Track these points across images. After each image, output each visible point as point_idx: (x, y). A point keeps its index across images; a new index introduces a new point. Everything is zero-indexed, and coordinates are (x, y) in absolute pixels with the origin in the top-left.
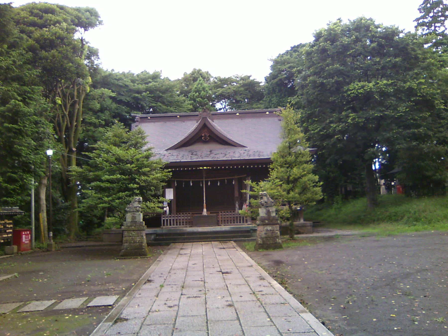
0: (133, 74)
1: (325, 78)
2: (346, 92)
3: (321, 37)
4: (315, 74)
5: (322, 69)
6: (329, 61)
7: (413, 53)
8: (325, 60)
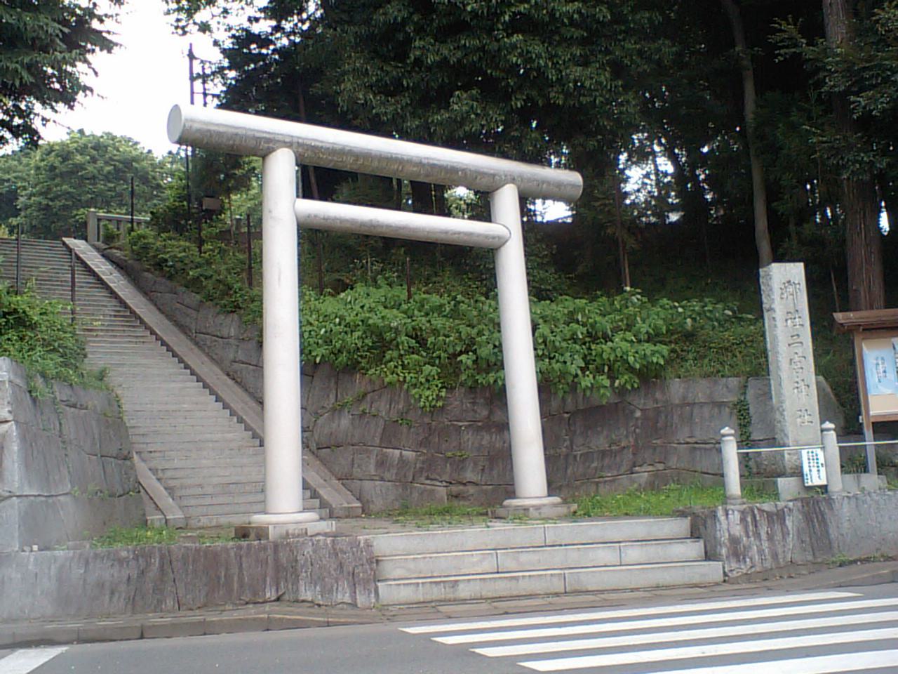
0: (101, 50)
1: (52, 200)
2: (74, 217)
3: (53, 151)
4: (41, 194)
5: (49, 189)
6: (57, 181)
7: (154, 182)
8: (54, 179)
